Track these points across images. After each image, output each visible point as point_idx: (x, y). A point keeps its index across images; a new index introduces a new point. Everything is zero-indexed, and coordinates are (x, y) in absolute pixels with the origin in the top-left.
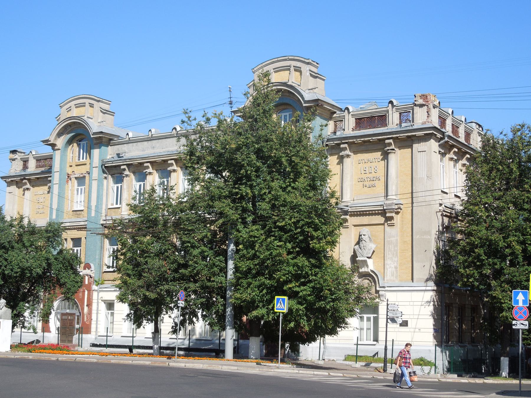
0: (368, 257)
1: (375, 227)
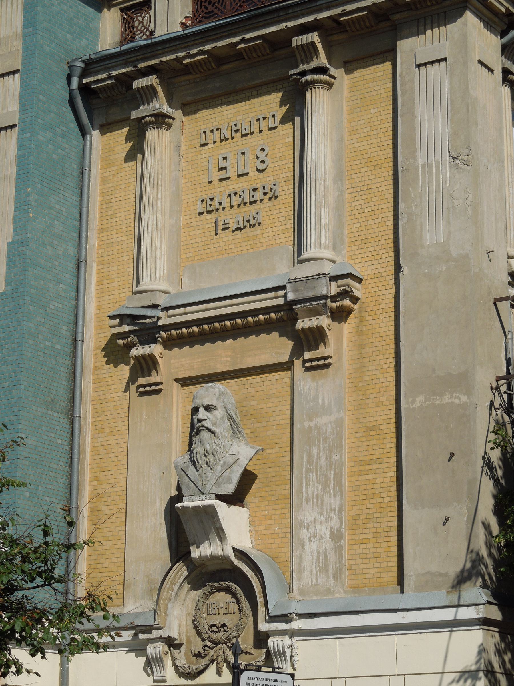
0: (219, 497)
1: (257, 379)
